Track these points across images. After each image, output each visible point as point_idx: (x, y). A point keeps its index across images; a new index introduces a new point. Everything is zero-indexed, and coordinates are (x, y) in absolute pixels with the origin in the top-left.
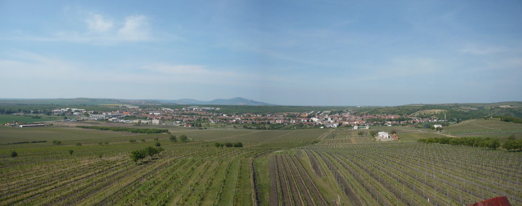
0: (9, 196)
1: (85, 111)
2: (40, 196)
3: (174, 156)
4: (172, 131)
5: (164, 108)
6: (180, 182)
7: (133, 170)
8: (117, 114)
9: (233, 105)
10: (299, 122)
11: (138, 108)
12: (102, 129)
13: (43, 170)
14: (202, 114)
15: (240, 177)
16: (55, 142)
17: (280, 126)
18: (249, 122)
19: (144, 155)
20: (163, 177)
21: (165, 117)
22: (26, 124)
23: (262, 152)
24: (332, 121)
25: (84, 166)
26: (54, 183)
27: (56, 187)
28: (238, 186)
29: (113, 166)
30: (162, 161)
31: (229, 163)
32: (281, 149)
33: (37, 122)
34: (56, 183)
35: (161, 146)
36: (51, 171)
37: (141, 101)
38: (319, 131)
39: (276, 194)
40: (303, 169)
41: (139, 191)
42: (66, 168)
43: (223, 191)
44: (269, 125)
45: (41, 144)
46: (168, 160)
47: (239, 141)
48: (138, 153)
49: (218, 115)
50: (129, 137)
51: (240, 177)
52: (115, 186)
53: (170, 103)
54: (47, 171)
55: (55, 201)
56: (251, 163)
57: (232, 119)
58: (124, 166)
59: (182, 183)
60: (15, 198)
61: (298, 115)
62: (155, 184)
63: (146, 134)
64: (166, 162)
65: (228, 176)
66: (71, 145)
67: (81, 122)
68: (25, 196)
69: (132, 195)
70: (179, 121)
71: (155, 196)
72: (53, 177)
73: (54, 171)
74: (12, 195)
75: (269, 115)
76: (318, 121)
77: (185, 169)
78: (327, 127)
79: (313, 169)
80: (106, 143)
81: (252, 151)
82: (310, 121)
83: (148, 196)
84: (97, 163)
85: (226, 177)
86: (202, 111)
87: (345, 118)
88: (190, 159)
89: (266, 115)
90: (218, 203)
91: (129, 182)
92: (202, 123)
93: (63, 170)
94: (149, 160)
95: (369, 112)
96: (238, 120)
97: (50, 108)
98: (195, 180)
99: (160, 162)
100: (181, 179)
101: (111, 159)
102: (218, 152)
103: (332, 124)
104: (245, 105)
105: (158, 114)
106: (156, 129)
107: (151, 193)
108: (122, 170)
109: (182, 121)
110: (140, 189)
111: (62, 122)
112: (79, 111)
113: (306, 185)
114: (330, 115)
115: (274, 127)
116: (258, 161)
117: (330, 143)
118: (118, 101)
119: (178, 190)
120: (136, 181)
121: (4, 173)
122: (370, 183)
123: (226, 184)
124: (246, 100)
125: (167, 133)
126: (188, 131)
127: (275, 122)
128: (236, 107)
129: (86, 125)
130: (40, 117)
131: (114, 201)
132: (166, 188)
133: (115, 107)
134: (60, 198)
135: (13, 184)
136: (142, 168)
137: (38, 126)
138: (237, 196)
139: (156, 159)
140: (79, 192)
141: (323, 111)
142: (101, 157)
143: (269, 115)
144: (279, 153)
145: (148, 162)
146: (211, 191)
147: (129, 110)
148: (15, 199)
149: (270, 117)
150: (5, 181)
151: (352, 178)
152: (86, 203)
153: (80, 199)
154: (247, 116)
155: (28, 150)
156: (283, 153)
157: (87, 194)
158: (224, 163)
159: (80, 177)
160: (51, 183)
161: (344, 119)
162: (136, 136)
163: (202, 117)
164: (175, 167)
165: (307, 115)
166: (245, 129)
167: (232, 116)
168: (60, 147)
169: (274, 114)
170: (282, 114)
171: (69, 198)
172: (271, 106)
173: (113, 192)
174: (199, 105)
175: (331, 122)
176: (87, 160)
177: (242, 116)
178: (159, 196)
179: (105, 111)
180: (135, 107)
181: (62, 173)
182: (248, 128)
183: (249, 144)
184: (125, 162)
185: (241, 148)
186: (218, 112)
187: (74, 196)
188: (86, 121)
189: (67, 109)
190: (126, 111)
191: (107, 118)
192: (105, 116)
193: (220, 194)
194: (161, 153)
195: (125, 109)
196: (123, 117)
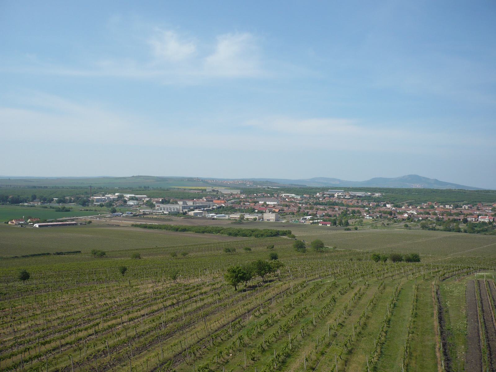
0: (15, 350)
1: (148, 199)
2: (68, 348)
3: (302, 276)
5: (285, 193)
6: (312, 322)
7: (231, 300)
8: (202, 203)
9: (404, 187)
11: (239, 193)
12: (177, 230)
13: (75, 302)
14: (350, 204)
15: (416, 314)
16: (95, 253)
17: (486, 227)
19: (250, 274)
20: (282, 313)
21: (286, 209)
22: (45, 221)
23: (453, 271)
25: (145, 294)
26: (94, 325)
27: (96, 333)
28: (412, 330)
29: (195, 293)
30: (278, 286)
31: (397, 290)
32: (488, 269)
33: (64, 218)
34: (98, 324)
35: (279, 259)
36: (88, 304)
37: (244, 181)
39: (478, 351)
41: (241, 336)
42: (114, 298)
43: (386, 338)
44: (465, 225)
45: (71, 256)
46: (292, 284)
48: (238, 272)
50: (223, 244)
51: (416, 314)
52: (199, 329)
53: (295, 185)
54: (81, 304)
55: (95, 357)
56: (435, 290)
59: (314, 323)
60: (26, 353)
62: (269, 325)
63: (253, 238)
65: (395, 312)
66: (123, 259)
67: (141, 218)
68: (43, 349)
69: (229, 344)
70: (310, 215)
71: (268, 346)
72: (92, 314)
73: (94, 304)
74: (22, 348)
75: (467, 207)
77: (321, 299)
80: (184, 254)
81: (437, 270)
83: (256, 345)
84: (168, 288)
85: (391, 314)
86: (349, 199)
88: (329, 281)
90: (378, 360)
91: (223, 321)
92: (350, 219)
93: (109, 302)
94: (258, 283)
96: (412, 214)
97: (86, 192)
98: (338, 318)
99: (278, 287)
100: (313, 316)
101: (192, 281)
105: (274, 203)
107: (262, 340)
108: (210, 300)
109: (315, 215)
110: (242, 333)
111: (107, 218)
112: (137, 199)
115: (475, 228)
116: (447, 287)
118: (205, 182)
119: (309, 335)
120: (236, 319)
121: (7, 309)
123: (391, 326)
125: (289, 237)
126: (325, 232)
127: (476, 219)
128: (409, 191)
129: (149, 223)
130: (70, 208)
131: (197, 355)
132: (287, 332)
133: (199, 191)
134: (103, 351)
135: (23, 329)
136: (246, 297)
137: (66, 225)
138: (410, 347)
139: (270, 281)
140: (136, 340)
142: (175, 278)
143: (467, 207)
144: (483, 276)
145: (256, 286)
146: (365, 338)
147: (224, 197)
148: (27, 355)
149: (468, 210)
150: (9, 324)
152: (150, 359)
153: (138, 352)
154: (428, 208)
155: (49, 268)
156: (491, 278)
157: (150, 342)
158: (388, 289)
159: (139, 314)
160: (90, 325)
162: (235, 242)
163: (350, 209)
164: (303, 296)
166: (424, 231)
167: (402, 207)
168: (104, 261)
169: (475, 205)
170: (490, 206)
171: (120, 351)
172: (470, 191)
173: (196, 339)
174: (345, 188)
176: (150, 283)
177: (418, 207)
178: (276, 346)
179: (182, 199)
180: (235, 192)
181: (107, 307)
182: (429, 229)
184: (217, 286)
185: (417, 263)
186: (377, 200)
187: (127, 348)
188: (148, 216)
189: (116, 194)
190: (219, 199)
191: (185, 210)
193: (381, 343)
194: (279, 272)
195: (216, 195)
196: (213, 209)
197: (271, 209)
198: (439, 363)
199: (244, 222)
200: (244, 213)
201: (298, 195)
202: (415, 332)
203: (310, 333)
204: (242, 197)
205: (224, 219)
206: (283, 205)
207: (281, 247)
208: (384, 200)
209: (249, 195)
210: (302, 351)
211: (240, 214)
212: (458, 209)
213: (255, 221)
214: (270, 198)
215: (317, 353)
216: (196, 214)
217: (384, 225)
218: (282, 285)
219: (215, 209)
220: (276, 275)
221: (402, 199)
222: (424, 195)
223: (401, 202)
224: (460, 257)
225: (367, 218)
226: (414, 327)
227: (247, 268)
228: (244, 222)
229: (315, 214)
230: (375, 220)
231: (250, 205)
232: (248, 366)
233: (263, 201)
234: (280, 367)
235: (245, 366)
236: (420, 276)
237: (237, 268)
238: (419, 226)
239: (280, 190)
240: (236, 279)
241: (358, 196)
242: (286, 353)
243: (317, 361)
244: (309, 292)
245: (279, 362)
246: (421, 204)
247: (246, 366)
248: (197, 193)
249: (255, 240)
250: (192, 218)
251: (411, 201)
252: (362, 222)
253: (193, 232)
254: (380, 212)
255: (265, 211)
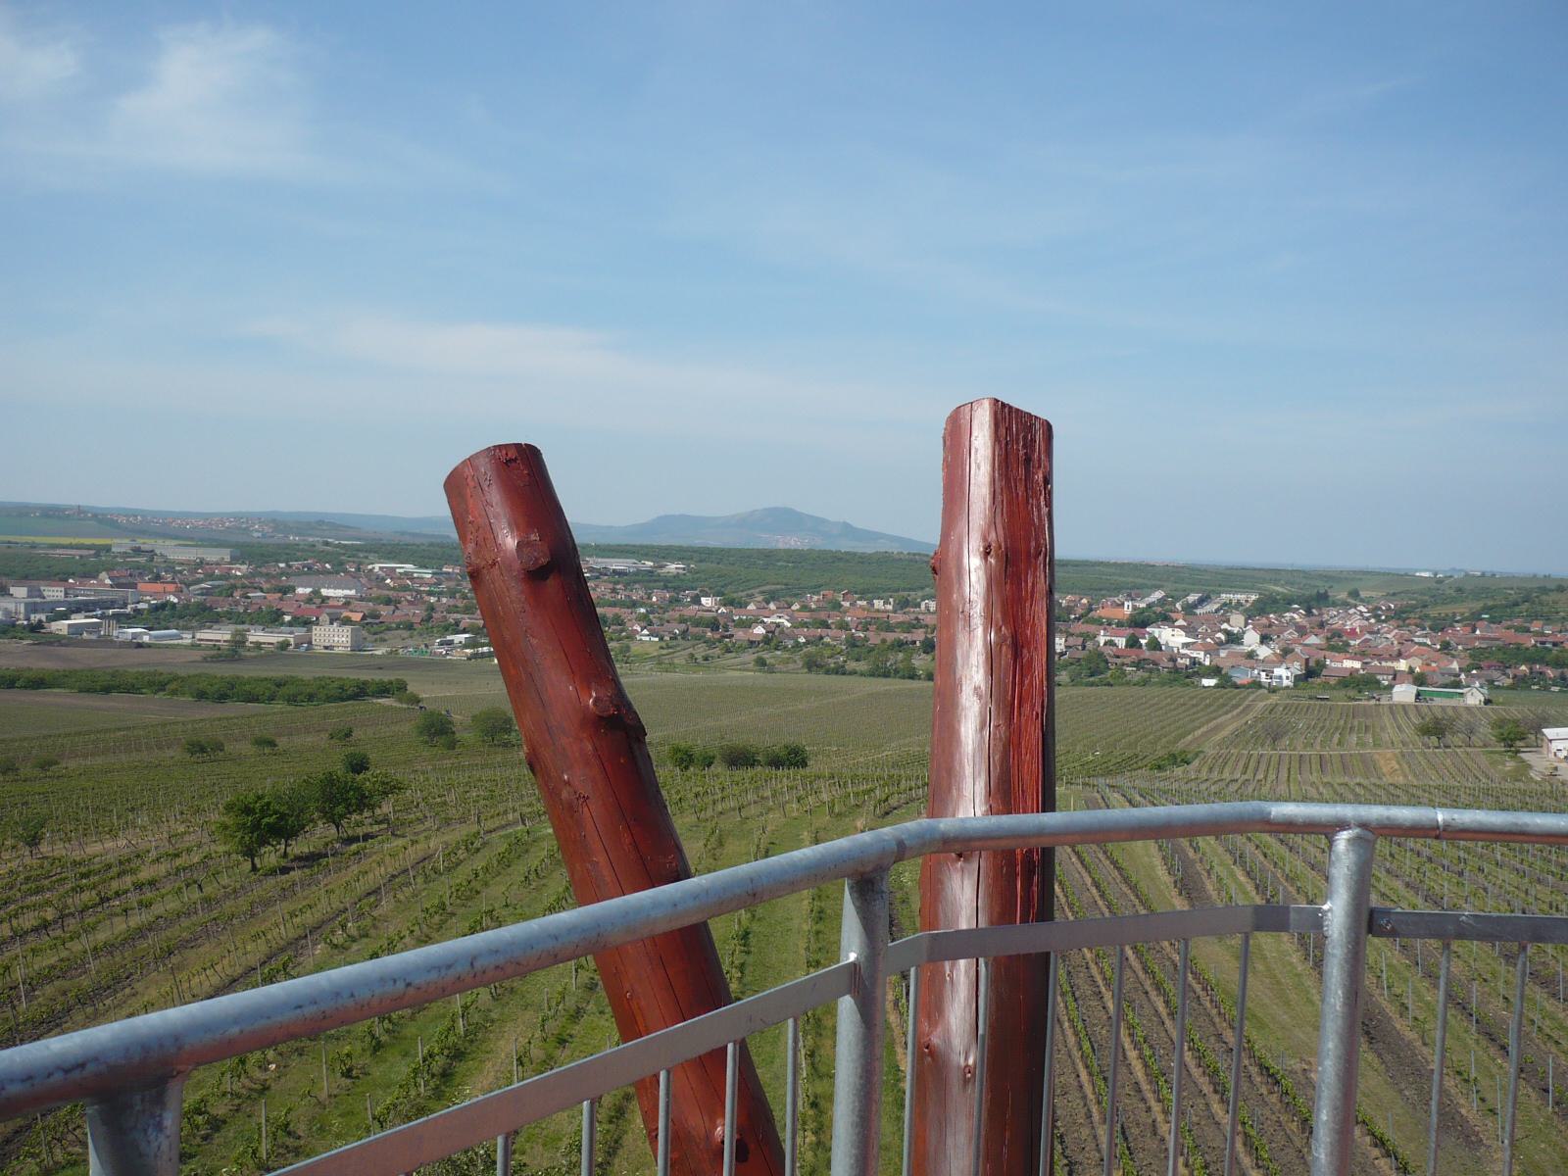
3: (463, 820)
4: (428, 690)
10: (1084, 648)
11: (227, 559)
18: (834, 639)
20: (417, 933)
21: (385, 611)
23: (910, 790)
24: (1264, 652)
29: (115, 885)
30: (387, 856)
37: (242, 521)
38: (1194, 702)
40: (1125, 889)
44: (929, 657)
47: (791, 740)
49: (675, 601)
57: (746, 625)
58: (187, 886)
61: (1080, 611)
63: (279, 706)
64: (421, 855)
70: (464, 631)
71: (387, 1031)
76: (1186, 645)
78: (1239, 682)
79: (1180, 894)
80: (45, 765)
82: (1143, 642)
87: (1340, 636)
89: (919, 605)
95: (1487, 609)
96: (778, 625)
101: (94, 849)
102: (697, 795)
103: (1268, 666)
104: (811, 551)
106: (340, 679)
108: (173, 905)
113: (1145, 970)
114: (1252, 613)
117: (1256, 769)
118: (105, 520)
122: (1505, 998)
123: (752, 949)
124: (817, 524)
125: (400, 701)
128: (769, 556)
133: (85, 552)
139: (367, 837)
141: (1219, 593)
142: (34, 841)
147: (176, 572)
151: (1395, 962)
161: (1338, 642)
162: (220, 719)
164: (477, 875)
165: (1128, 608)
166: (813, 676)
167: (747, 604)
175: (1261, 658)
177: (796, 607)
178: (414, 1030)
179: (23, 578)
180: (212, 555)
182: (827, 672)
183: (837, 754)
186: (673, 584)
190: (157, 578)
191: (35, 618)
192: (22, 609)
194: (386, 808)
195: (146, 567)
196: (136, 610)
197: (338, 611)
198: (897, 1041)
199: (248, 654)
200: (246, 627)
201: (427, 568)
202: (822, 961)
203: (515, 984)
204: (238, 573)
205: (178, 645)
206: (377, 600)
207: (374, 734)
208: (694, 585)
209: (260, 567)
210: (498, 1039)
211: (233, 627)
212: (909, 612)
213: (284, 652)
214: (331, 577)
215: (545, 1040)
216: (77, 629)
217: (696, 659)
218: (405, 848)
219: (146, 612)
220: (381, 818)
221: (748, 581)
222: (812, 570)
223: (742, 591)
224: (919, 751)
225: (644, 638)
226: (820, 949)
227: (290, 798)
228: (248, 654)
229: (479, 628)
230: (667, 645)
231: (265, 598)
232: (335, 1096)
233: (310, 587)
234: (437, 1087)
235: (323, 1095)
236: (818, 807)
237: (259, 798)
238: (798, 662)
239: (366, 551)
240: (255, 835)
241: (614, 570)
242: (449, 1049)
243: (548, 1064)
244: (495, 863)
245: (433, 1076)
246: (802, 595)
247: (330, 1096)
248: (78, 557)
249: (289, 712)
250: (63, 641)
251: (773, 587)
252: (629, 651)
253: (72, 688)
254: (682, 621)
255: (317, 619)
